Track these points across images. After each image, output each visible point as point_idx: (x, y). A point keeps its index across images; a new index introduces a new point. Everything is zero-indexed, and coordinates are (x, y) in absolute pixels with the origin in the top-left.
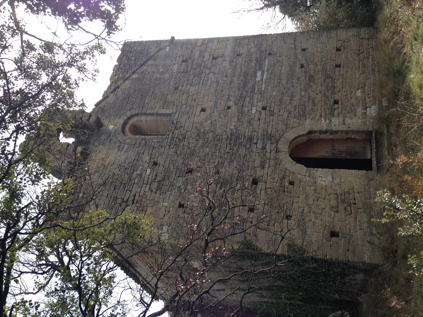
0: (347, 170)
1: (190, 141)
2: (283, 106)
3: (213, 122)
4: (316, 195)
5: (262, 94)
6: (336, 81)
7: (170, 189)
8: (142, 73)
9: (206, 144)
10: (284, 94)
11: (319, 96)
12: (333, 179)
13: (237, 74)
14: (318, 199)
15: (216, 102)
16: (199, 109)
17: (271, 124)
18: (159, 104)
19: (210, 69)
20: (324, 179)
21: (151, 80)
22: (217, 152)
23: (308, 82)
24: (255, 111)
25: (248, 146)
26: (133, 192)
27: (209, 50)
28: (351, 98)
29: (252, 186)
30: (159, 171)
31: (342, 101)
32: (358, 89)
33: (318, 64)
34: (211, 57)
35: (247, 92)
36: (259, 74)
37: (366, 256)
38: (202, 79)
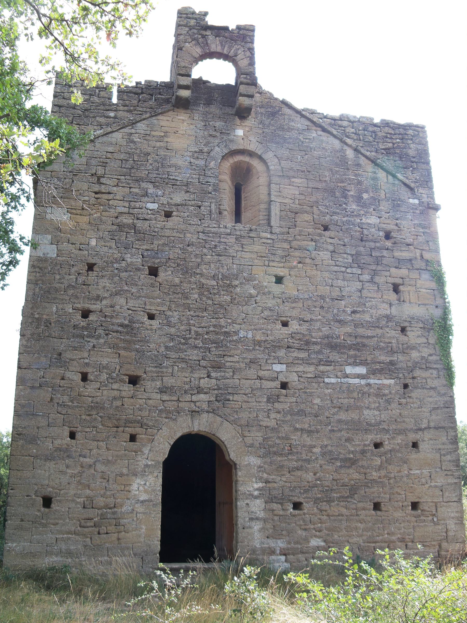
0: (161, 509)
1: (212, 265)
2: (289, 417)
3: (253, 299)
4: (112, 476)
5: (314, 380)
6: (342, 504)
7: (119, 245)
8: (358, 165)
9: (206, 293)
10: (316, 416)
11: (310, 477)
12: (142, 502)
13: (361, 331)
14: (105, 479)
15: (296, 300)
16: (281, 272)
17: (250, 400)
18: (291, 201)
19: (372, 281)
20: (141, 488)
21: (342, 182)
22: (192, 313)
23: (342, 456)
24: (278, 370)
25: (203, 363)
26: (115, 188)
27: (414, 275)
28: (305, 530)
29: (127, 375)
30: (154, 222)
31: (299, 515)
32: (325, 541)
33: (381, 471)
34: (399, 281)
35: (319, 352)
36: (362, 370)
37: (14, 545)
38: (349, 270)
